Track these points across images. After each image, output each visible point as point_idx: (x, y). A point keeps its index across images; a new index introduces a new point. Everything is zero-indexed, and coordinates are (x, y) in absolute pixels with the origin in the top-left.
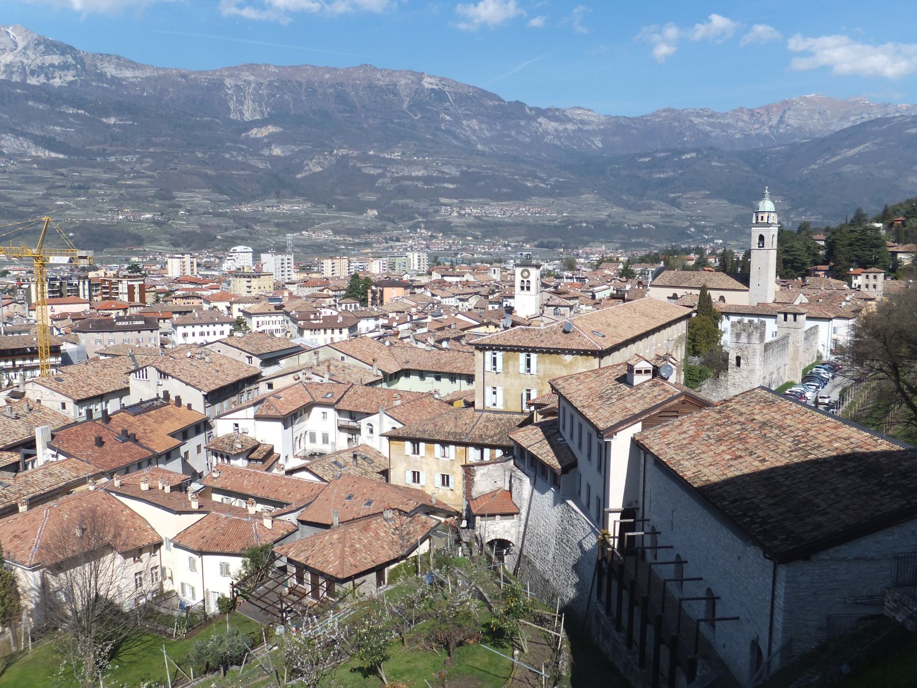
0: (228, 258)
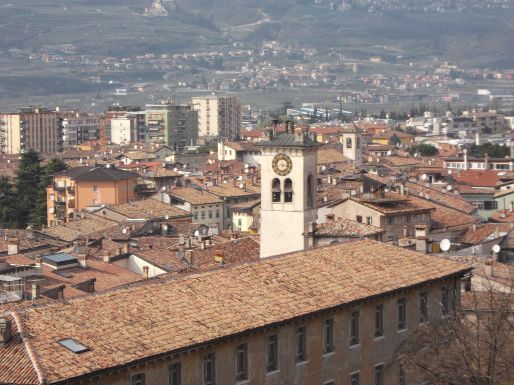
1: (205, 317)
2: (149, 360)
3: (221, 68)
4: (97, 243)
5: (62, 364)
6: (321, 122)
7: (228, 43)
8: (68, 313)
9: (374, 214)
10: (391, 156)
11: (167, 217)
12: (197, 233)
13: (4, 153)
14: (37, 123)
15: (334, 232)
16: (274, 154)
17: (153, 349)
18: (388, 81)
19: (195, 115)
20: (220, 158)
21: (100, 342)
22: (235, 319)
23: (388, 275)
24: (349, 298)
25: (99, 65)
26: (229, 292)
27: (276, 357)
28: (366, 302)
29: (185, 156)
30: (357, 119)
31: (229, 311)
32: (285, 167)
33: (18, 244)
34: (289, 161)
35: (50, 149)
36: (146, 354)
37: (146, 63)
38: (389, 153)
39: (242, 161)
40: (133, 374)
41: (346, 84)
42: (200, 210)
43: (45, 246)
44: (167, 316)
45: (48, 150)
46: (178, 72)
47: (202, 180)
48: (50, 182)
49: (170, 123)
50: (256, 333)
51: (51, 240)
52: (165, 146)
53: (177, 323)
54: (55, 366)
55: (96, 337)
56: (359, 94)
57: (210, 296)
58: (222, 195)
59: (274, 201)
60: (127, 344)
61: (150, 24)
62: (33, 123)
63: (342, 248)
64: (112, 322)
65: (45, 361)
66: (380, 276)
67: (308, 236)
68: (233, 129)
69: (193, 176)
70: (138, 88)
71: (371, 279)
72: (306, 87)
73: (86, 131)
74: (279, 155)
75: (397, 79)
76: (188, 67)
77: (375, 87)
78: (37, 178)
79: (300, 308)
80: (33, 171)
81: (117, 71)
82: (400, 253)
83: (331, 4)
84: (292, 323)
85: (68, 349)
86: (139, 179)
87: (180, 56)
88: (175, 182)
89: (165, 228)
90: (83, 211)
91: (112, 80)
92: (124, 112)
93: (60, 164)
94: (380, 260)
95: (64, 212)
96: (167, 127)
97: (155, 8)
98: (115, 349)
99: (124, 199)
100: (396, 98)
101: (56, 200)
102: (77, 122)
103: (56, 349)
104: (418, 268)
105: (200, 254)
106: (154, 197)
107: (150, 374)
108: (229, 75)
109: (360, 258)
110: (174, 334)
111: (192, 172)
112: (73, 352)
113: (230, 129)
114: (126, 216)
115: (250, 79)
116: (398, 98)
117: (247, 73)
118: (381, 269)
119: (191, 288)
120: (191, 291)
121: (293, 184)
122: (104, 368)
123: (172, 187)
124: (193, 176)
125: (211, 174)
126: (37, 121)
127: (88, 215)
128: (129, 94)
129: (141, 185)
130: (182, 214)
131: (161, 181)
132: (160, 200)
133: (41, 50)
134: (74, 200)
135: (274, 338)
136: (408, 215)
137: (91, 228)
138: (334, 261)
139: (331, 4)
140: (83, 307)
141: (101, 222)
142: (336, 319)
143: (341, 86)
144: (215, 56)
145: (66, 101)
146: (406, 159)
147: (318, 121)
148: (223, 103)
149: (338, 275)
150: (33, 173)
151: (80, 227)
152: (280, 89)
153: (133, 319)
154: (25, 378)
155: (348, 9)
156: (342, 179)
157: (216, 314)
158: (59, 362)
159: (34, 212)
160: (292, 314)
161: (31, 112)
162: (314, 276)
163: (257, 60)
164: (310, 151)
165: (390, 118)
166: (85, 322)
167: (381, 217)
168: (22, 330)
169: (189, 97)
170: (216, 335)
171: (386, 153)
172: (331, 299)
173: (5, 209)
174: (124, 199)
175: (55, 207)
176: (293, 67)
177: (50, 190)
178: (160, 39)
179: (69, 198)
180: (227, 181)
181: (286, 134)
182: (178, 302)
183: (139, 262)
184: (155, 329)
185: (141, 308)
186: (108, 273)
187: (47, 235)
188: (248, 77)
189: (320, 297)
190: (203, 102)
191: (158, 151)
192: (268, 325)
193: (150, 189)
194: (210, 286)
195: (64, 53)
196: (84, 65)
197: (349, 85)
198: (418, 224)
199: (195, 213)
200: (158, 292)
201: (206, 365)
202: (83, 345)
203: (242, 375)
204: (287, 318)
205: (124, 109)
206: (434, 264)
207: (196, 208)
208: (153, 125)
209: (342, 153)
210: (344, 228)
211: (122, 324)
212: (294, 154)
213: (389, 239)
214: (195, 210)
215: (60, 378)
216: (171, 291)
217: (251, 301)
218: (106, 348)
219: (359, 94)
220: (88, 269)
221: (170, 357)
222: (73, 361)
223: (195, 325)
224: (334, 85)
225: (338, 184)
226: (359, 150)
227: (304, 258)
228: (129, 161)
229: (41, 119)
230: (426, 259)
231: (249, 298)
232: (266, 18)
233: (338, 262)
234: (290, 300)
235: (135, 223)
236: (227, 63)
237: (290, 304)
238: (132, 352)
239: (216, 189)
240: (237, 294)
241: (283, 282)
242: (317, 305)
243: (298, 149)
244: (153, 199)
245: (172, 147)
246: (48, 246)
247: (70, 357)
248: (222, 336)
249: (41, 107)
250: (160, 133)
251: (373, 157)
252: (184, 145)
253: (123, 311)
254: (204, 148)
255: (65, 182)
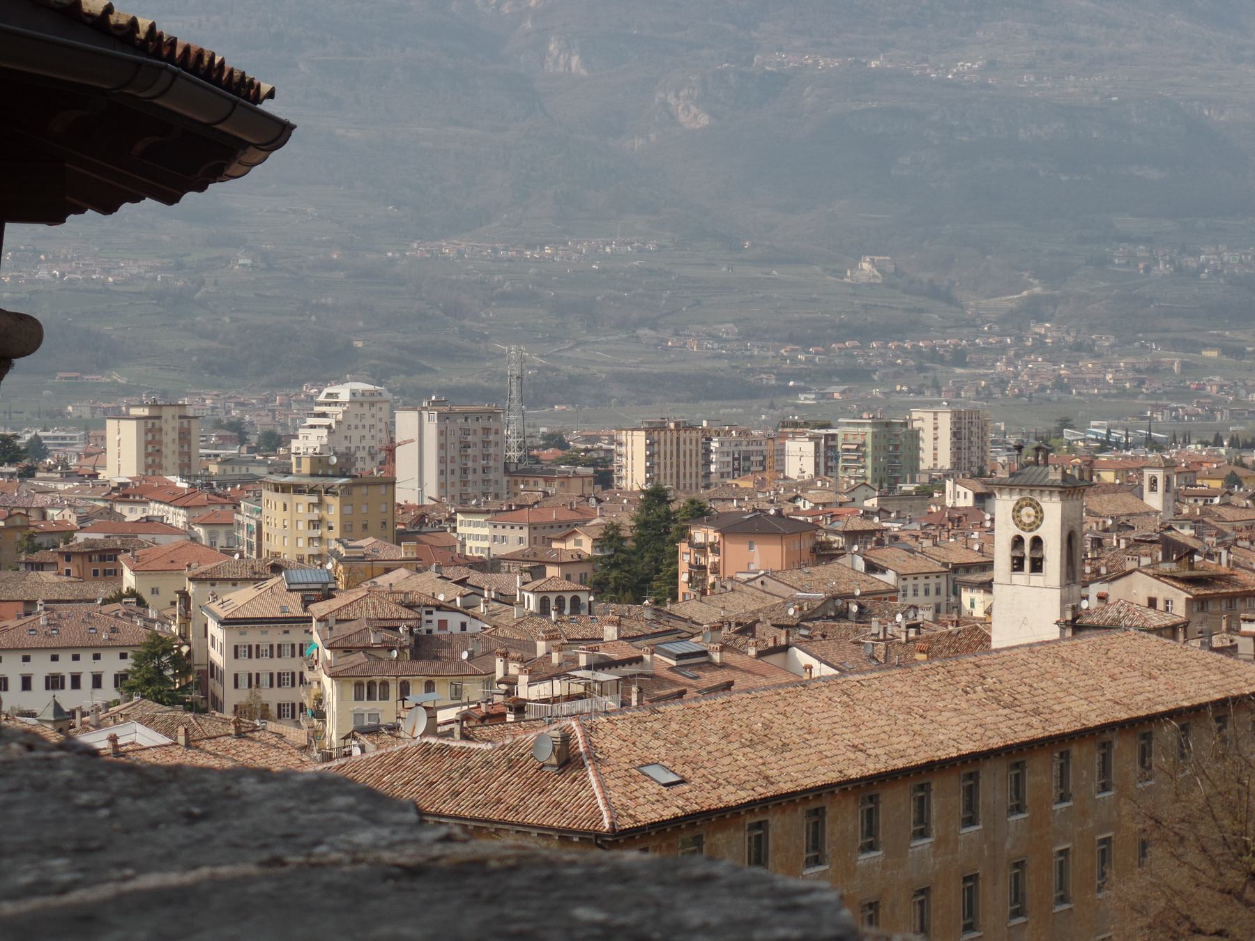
0: (311, 421)
1: (867, 739)
2: (775, 800)
3: (963, 364)
4: (746, 629)
5: (641, 800)
6: (1116, 451)
7: (975, 326)
8: (657, 726)
9: (1176, 594)
10: (1220, 505)
11: (858, 593)
12: (899, 618)
13: (621, 488)
14: (671, 444)
15: (1106, 621)
16: (1016, 497)
17: (781, 785)
18: (1231, 388)
19: (915, 436)
20: (949, 503)
21: (702, 771)
22: (911, 744)
23: (1162, 687)
24: (1095, 720)
25: (773, 357)
26: (907, 703)
27: (977, 806)
28: (1124, 727)
29: (895, 498)
30: (1176, 447)
31: (904, 732)
32: (1032, 519)
33: (619, 625)
34: (1038, 508)
35: (691, 485)
36: (770, 791)
37: (846, 355)
38: (1217, 500)
39: (984, 510)
40: (750, 820)
41: (1161, 391)
42: (910, 582)
43: (671, 630)
44: (807, 736)
45: (688, 485)
46: (896, 369)
47: (917, 537)
48: (684, 535)
49: (875, 448)
50: (944, 767)
51: (680, 622)
52: (865, 484)
53: (822, 748)
54: (630, 803)
55: (696, 763)
56: (1182, 408)
57: (877, 708)
58: (946, 561)
59: (1014, 570)
60: (742, 775)
61: (854, 295)
62: (665, 444)
63: (1092, 643)
64: (723, 741)
65: (617, 795)
66: (1149, 688)
67: (1064, 626)
68: (974, 459)
69: (905, 530)
70: (833, 393)
71: (1134, 691)
72: (1097, 395)
73: (747, 458)
74: (1024, 499)
75: (1245, 385)
76: (911, 363)
77: (1208, 396)
78: (665, 527)
79: (1016, 732)
80: (659, 516)
81: (802, 366)
82: (1185, 654)
83: (1141, 266)
84: (1003, 755)
85: (653, 779)
86: (820, 532)
87: (899, 345)
88: (874, 539)
89: (855, 608)
90: (731, 579)
91: (793, 380)
92: (805, 429)
93: (701, 507)
94: (1151, 664)
95: (704, 580)
96: (870, 454)
97: (862, 269)
98: (723, 782)
99: (794, 563)
100: (1244, 414)
101: (693, 562)
102: (733, 444)
103: (634, 779)
104: (1212, 677)
105: (900, 649)
106: (840, 561)
107: (777, 822)
108: (975, 374)
109: (1118, 659)
110: (815, 763)
111: (904, 524)
112: (660, 784)
113: (969, 459)
114: (796, 588)
115: (1009, 382)
116: (1246, 414)
117: (1003, 372)
118: (1151, 677)
119: (848, 696)
120: (847, 700)
121: (1044, 545)
122: (704, 809)
123: (869, 547)
124: (905, 530)
125: (933, 527)
126: (671, 441)
127: (736, 586)
128: (819, 403)
129: (823, 542)
130: (883, 588)
131: (853, 536)
132: (850, 566)
133: (686, 332)
134: (719, 562)
135: (973, 776)
136: (1231, 598)
137: (741, 606)
138: (1077, 662)
139: (1141, 266)
140: (680, 717)
141: (757, 597)
142: (1075, 750)
143: (1148, 396)
144: (954, 345)
145: (722, 411)
146: (1244, 510)
147: (1112, 449)
148: (960, 418)
149: (1081, 684)
150: (659, 520)
151: (726, 604)
152: (1055, 399)
153: (755, 738)
154: (585, 820)
155: (1167, 272)
156: (1136, 540)
157: (883, 736)
158: (638, 798)
159: (659, 579)
160: (1003, 740)
161: (662, 427)
162: (1043, 685)
163: (1021, 352)
164: (1073, 495)
165: (1230, 445)
166: (682, 739)
167: (1187, 599)
168: (586, 749)
169: (907, 408)
170: (881, 767)
171: (1212, 501)
172: (1066, 720)
173: (615, 573)
174: (794, 563)
175: (690, 573)
176: (1078, 364)
177: (683, 547)
178: (869, 318)
179: (712, 559)
180: (955, 539)
181: (1035, 468)
182: (826, 715)
183: (802, 658)
184: (787, 755)
185: (768, 722)
186: (754, 674)
187: (674, 615)
188: (1006, 379)
189: (1049, 716)
190: (929, 417)
191: (853, 490)
192: (963, 755)
193: (837, 549)
194: (878, 694)
195: (721, 337)
196: (751, 357)
197: (1165, 393)
198: (1246, 611)
199: (903, 586)
200: (796, 700)
201: (865, 812)
202: (675, 774)
203: (922, 830)
204: (995, 746)
205: (806, 424)
206: (1239, 672)
207: (905, 579)
208: (848, 450)
209: (1142, 499)
210: (1121, 615)
211: (737, 745)
212: (1046, 499)
213: (1201, 635)
214: (902, 583)
215: (636, 822)
216: (817, 698)
217: (939, 718)
218: (710, 780)
219: (1182, 408)
220: (723, 666)
221: (807, 798)
222: (658, 797)
223: (850, 751)
224: (1142, 393)
225: (1128, 547)
226: (1168, 495)
227: (1029, 657)
228: (809, 506)
229: (678, 438)
230: (1228, 665)
231: (937, 713)
232: (1036, 286)
233: (1083, 664)
234: (1001, 719)
235: (808, 599)
236: (974, 356)
237: (1001, 725)
238: (748, 787)
239: (936, 551)
240: (918, 707)
241: (992, 691)
242: (1044, 728)
243: (1044, 491)
244: (839, 564)
245: (876, 486)
246: (674, 631)
247: (655, 791)
248: (890, 769)
249: (678, 420)
250: (860, 463)
251: (1190, 506)
252: (897, 482)
253: (741, 726)
254: (925, 488)
255: (706, 536)
